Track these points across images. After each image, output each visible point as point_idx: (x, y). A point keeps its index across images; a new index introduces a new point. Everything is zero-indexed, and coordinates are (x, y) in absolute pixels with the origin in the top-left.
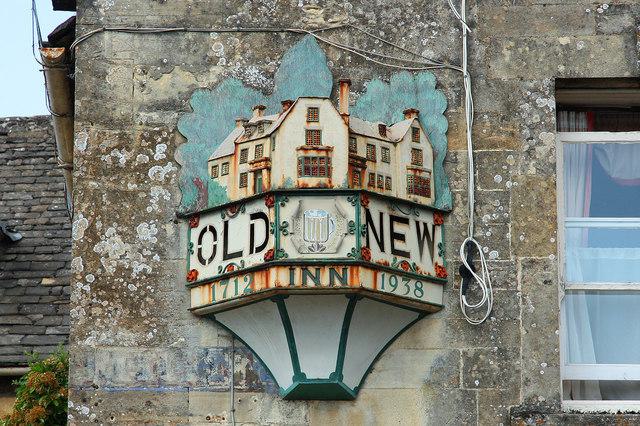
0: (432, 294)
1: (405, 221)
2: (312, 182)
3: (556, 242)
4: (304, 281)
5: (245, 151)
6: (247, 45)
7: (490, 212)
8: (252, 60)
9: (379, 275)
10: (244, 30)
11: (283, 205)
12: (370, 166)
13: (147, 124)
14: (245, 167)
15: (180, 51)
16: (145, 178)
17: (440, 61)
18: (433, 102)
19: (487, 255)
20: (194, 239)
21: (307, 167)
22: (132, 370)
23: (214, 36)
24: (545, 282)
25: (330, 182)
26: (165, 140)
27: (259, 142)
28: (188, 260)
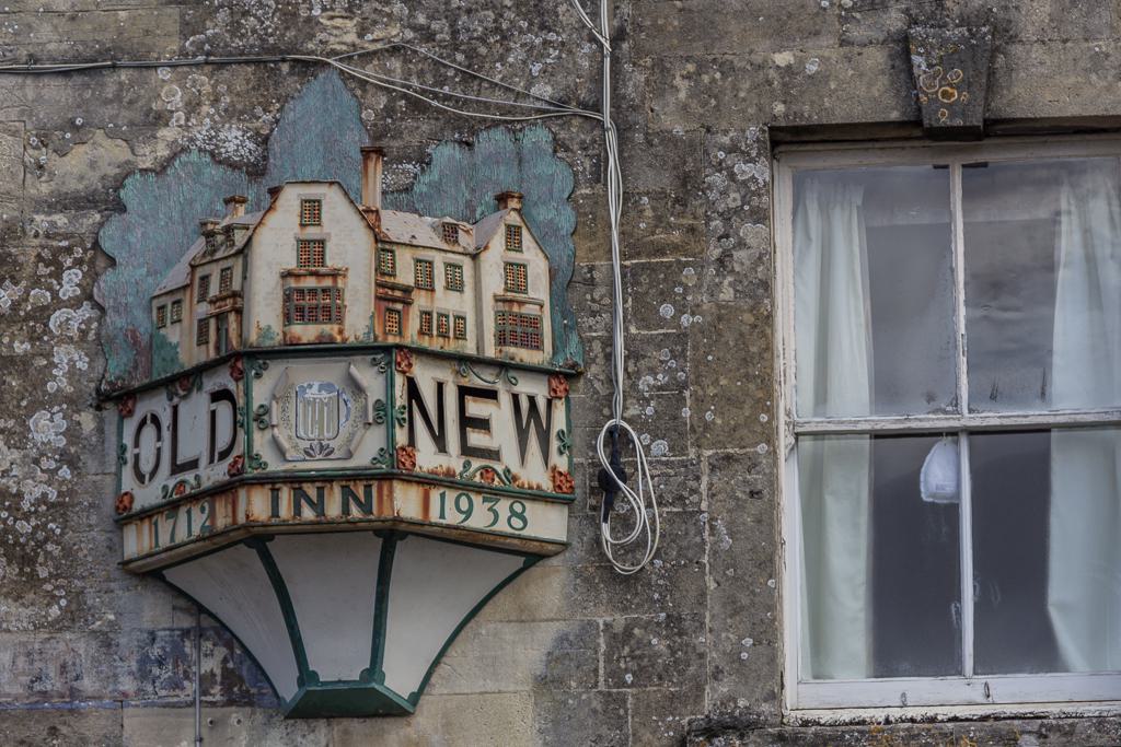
0: (548, 523)
1: (491, 395)
2: (306, 332)
3: (769, 422)
4: (346, 510)
5: (205, 279)
6: (222, 88)
7: (653, 372)
8: (231, 114)
9: (435, 495)
10: (218, 61)
11: (258, 376)
12: (420, 300)
13: (48, 236)
14: (204, 309)
15: (107, 102)
16: (45, 333)
17: (562, 102)
18: (552, 174)
19: (647, 448)
20: (128, 440)
21: (296, 307)
22: (23, 673)
23: (164, 74)
24: (752, 494)
25: (341, 332)
26: (78, 263)
27: (225, 264)
28: (118, 475)
